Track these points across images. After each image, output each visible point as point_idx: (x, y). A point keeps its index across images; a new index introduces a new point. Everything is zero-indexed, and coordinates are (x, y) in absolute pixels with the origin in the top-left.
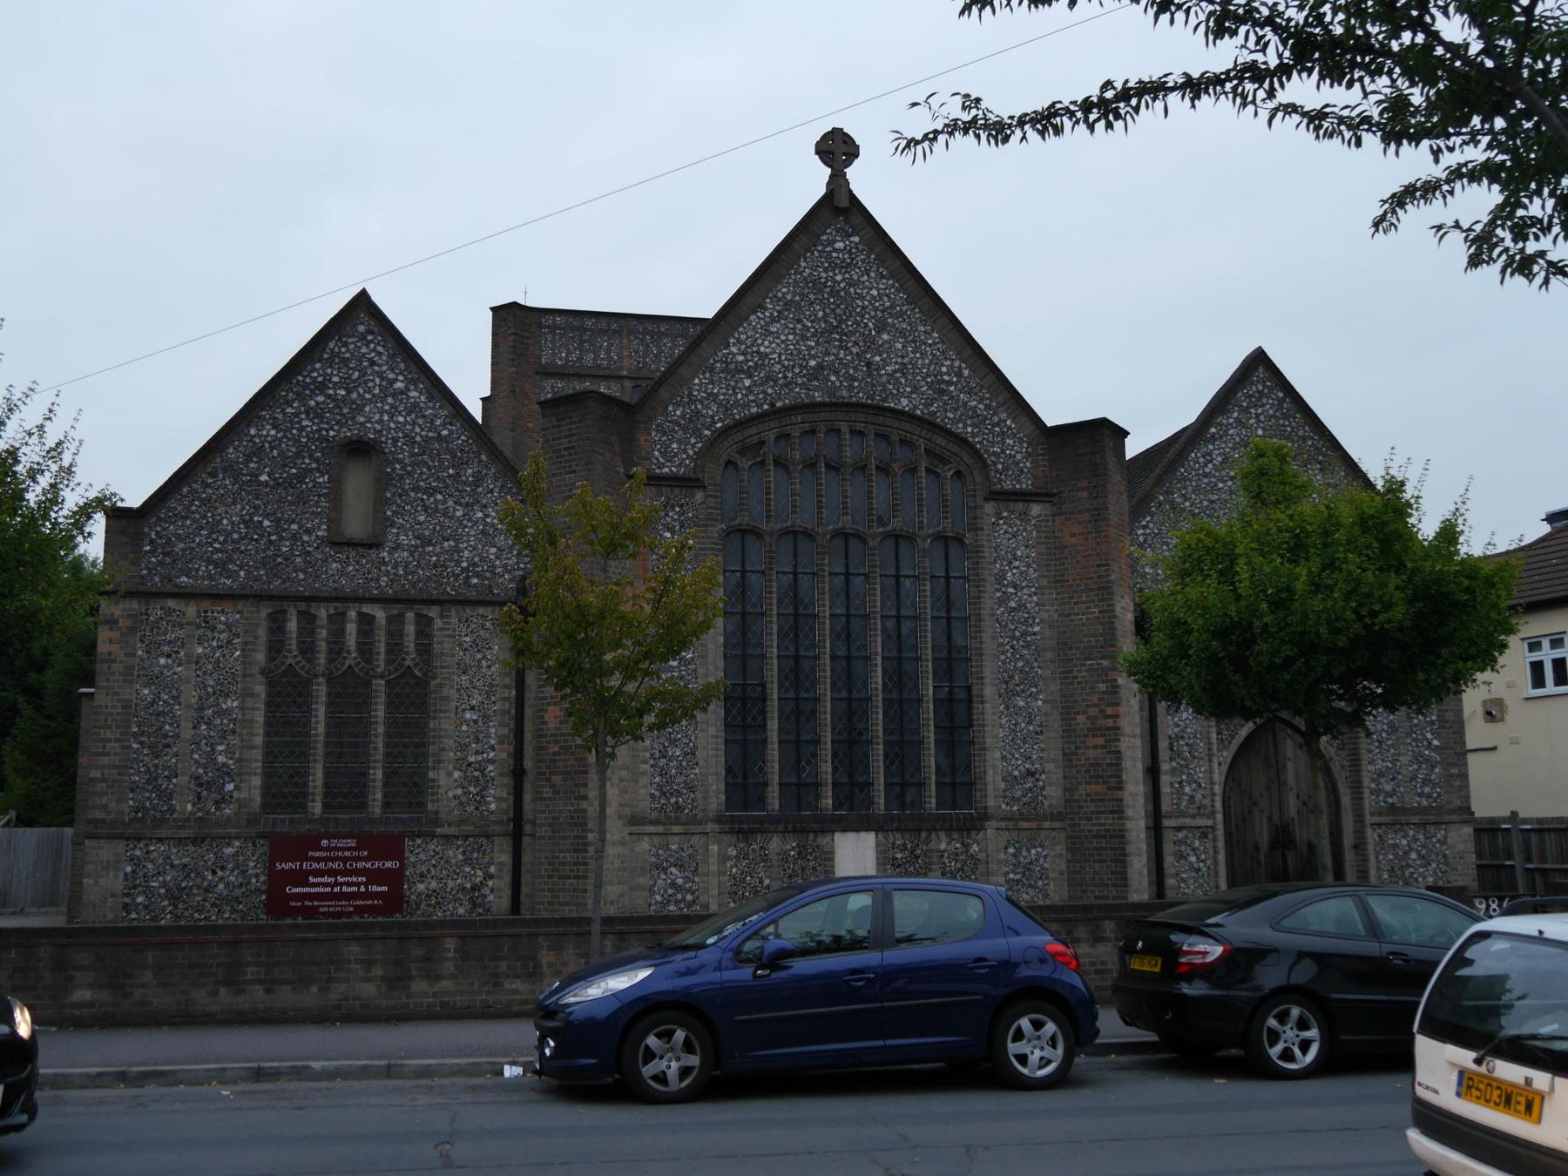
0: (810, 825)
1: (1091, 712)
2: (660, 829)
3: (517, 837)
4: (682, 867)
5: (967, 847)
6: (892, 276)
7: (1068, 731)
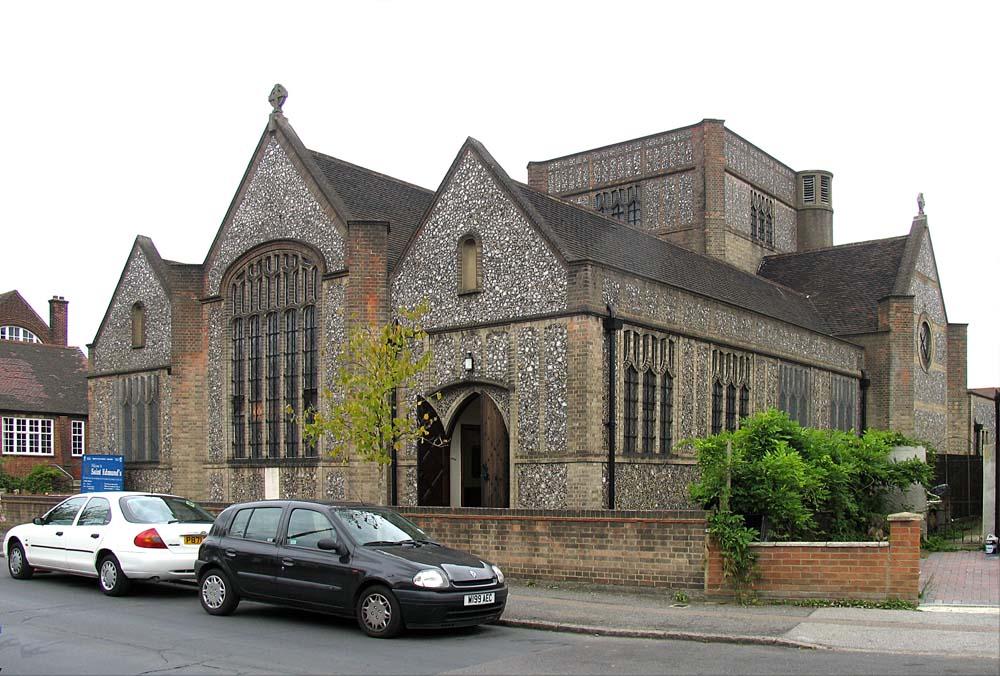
0: (258, 464)
4: (218, 483)
5: (312, 476)
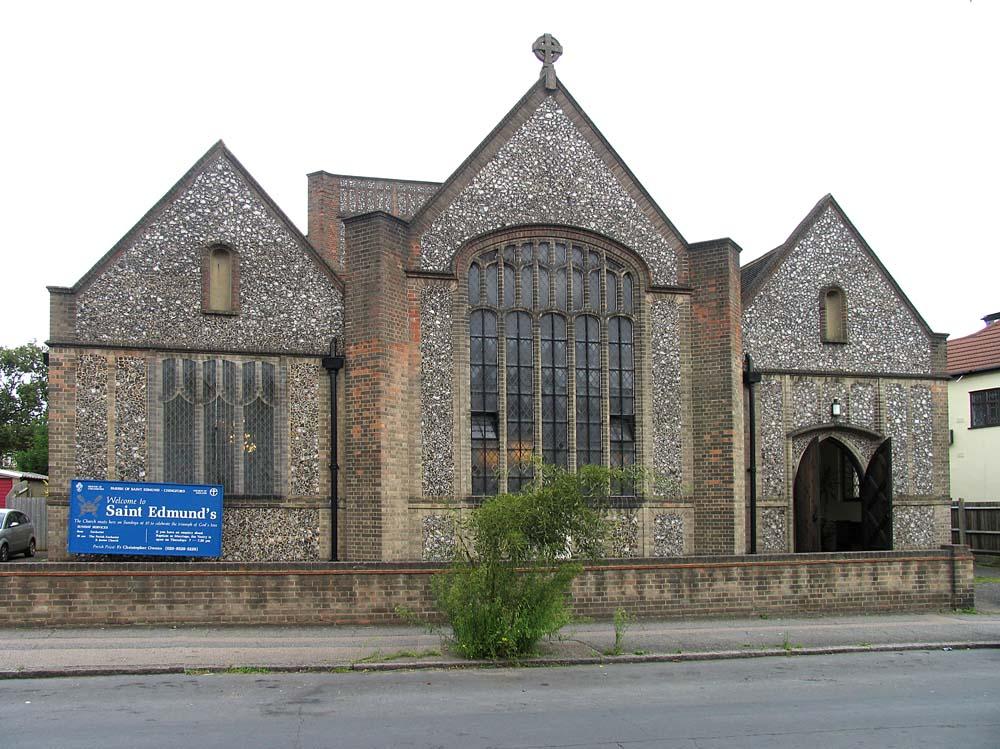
1: (713, 432)
2: (429, 506)
3: (334, 508)
6: (585, 137)
7: (698, 444)
